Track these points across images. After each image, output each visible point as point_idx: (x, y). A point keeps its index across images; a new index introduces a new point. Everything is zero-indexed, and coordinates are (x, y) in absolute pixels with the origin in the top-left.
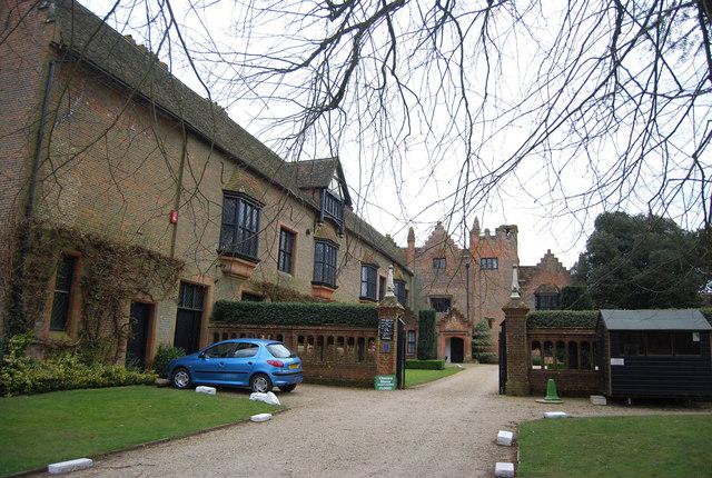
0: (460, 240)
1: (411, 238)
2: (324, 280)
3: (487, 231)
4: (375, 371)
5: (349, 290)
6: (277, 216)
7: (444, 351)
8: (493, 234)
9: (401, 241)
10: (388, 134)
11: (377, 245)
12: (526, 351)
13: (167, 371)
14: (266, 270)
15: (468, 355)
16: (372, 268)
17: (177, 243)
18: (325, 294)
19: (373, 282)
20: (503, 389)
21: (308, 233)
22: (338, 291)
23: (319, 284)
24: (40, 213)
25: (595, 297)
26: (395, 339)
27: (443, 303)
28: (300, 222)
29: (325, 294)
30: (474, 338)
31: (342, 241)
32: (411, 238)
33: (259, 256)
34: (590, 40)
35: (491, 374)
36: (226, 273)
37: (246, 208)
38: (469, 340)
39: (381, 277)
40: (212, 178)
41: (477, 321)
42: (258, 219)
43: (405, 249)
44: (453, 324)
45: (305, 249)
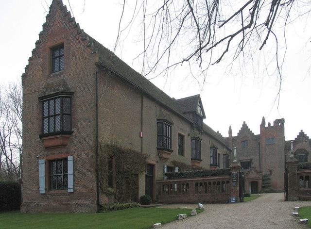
0: (256, 131)
1: (230, 132)
2: (197, 158)
3: (269, 124)
4: (229, 195)
5: (206, 163)
6: (179, 128)
7: (248, 189)
8: (272, 125)
9: (225, 135)
10: (46, 120)
11: (214, 137)
12: (297, 181)
13: (144, 201)
14: (175, 156)
15: (260, 188)
16: (214, 149)
17: (143, 146)
18: (197, 164)
19: (216, 156)
20: (287, 199)
21: (189, 135)
22: (202, 162)
23: (195, 159)
24: (101, 140)
25: (262, 186)
26: (239, 181)
27: (246, 165)
28: (186, 130)
29: (197, 164)
30: (263, 180)
31: (201, 137)
32: (230, 132)
33: (172, 149)
34: (136, 13)
35: (282, 196)
36: (160, 158)
37: (166, 127)
38: (260, 182)
39: (180, 135)
40: (152, 113)
41: (265, 172)
42: (171, 132)
43: (227, 138)
44: (253, 175)
45: (188, 141)
